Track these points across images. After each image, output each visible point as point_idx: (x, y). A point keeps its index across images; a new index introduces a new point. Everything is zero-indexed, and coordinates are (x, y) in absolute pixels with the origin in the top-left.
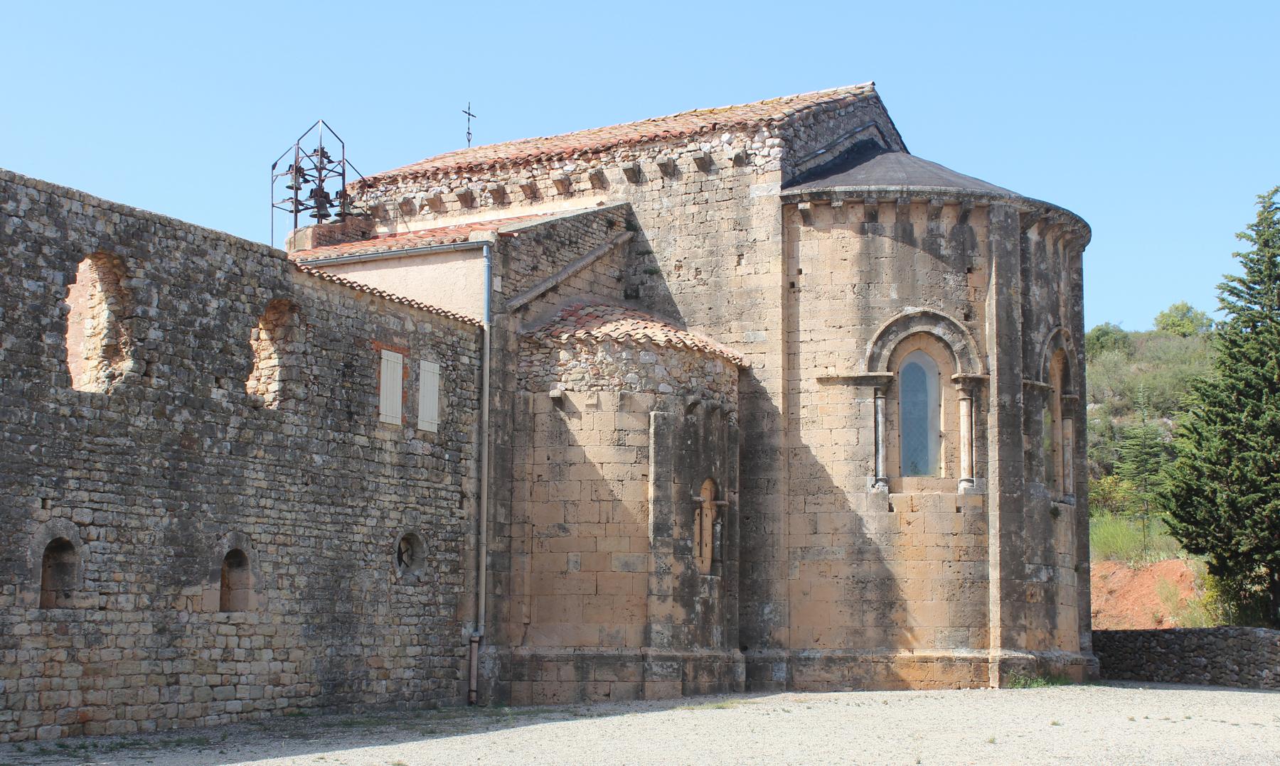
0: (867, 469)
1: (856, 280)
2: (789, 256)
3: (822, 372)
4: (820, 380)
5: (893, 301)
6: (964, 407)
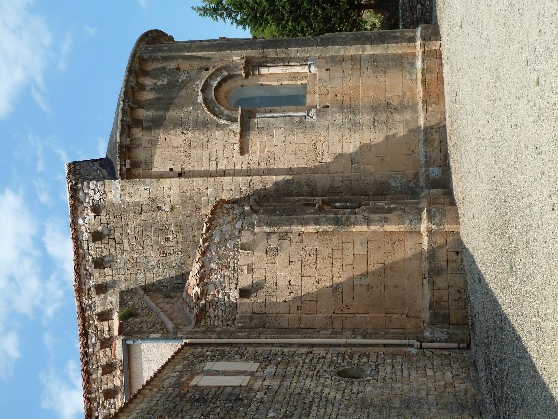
1: (179, 132)
2: (161, 176)
3: (237, 153)
4: (242, 153)
5: (193, 109)
6: (264, 71)
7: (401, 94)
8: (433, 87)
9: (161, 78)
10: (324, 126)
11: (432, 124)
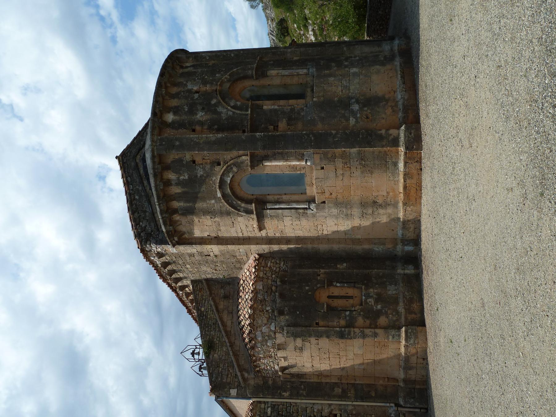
0: (304, 213)
1: (208, 217)
2: (202, 241)
7: (385, 194)
8: (413, 191)
9: (181, 172)
10: (323, 216)
11: (409, 219)
